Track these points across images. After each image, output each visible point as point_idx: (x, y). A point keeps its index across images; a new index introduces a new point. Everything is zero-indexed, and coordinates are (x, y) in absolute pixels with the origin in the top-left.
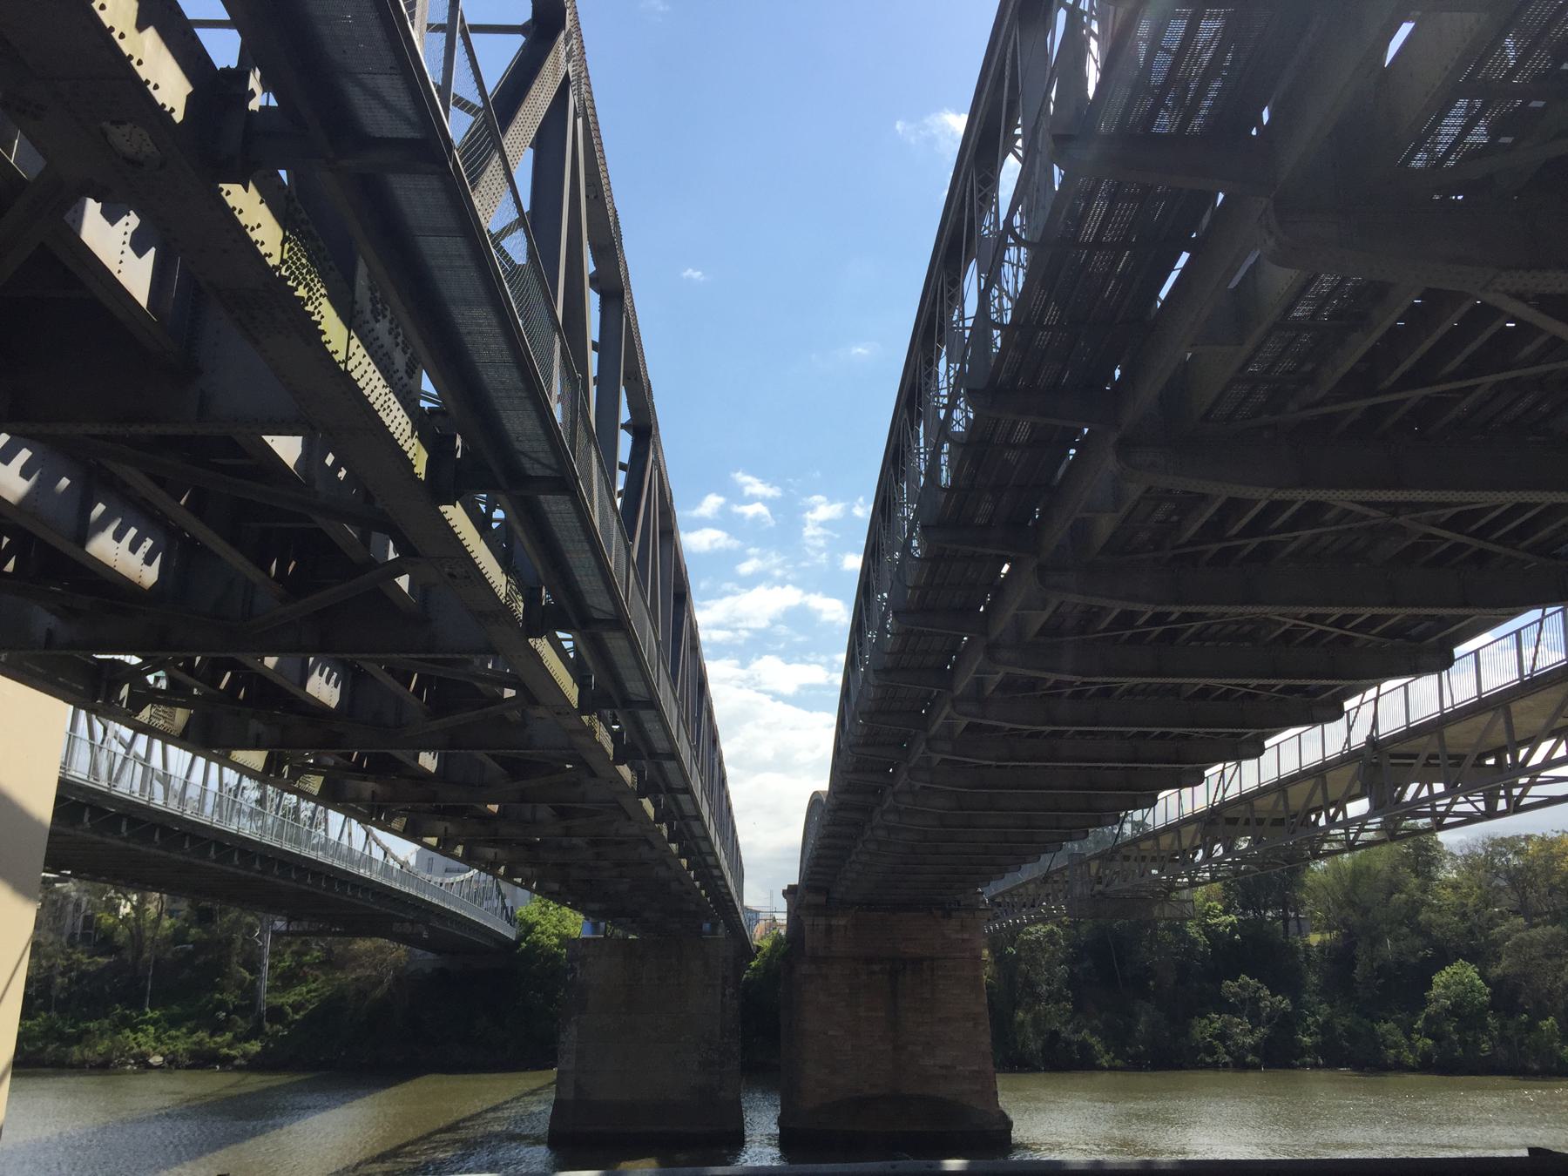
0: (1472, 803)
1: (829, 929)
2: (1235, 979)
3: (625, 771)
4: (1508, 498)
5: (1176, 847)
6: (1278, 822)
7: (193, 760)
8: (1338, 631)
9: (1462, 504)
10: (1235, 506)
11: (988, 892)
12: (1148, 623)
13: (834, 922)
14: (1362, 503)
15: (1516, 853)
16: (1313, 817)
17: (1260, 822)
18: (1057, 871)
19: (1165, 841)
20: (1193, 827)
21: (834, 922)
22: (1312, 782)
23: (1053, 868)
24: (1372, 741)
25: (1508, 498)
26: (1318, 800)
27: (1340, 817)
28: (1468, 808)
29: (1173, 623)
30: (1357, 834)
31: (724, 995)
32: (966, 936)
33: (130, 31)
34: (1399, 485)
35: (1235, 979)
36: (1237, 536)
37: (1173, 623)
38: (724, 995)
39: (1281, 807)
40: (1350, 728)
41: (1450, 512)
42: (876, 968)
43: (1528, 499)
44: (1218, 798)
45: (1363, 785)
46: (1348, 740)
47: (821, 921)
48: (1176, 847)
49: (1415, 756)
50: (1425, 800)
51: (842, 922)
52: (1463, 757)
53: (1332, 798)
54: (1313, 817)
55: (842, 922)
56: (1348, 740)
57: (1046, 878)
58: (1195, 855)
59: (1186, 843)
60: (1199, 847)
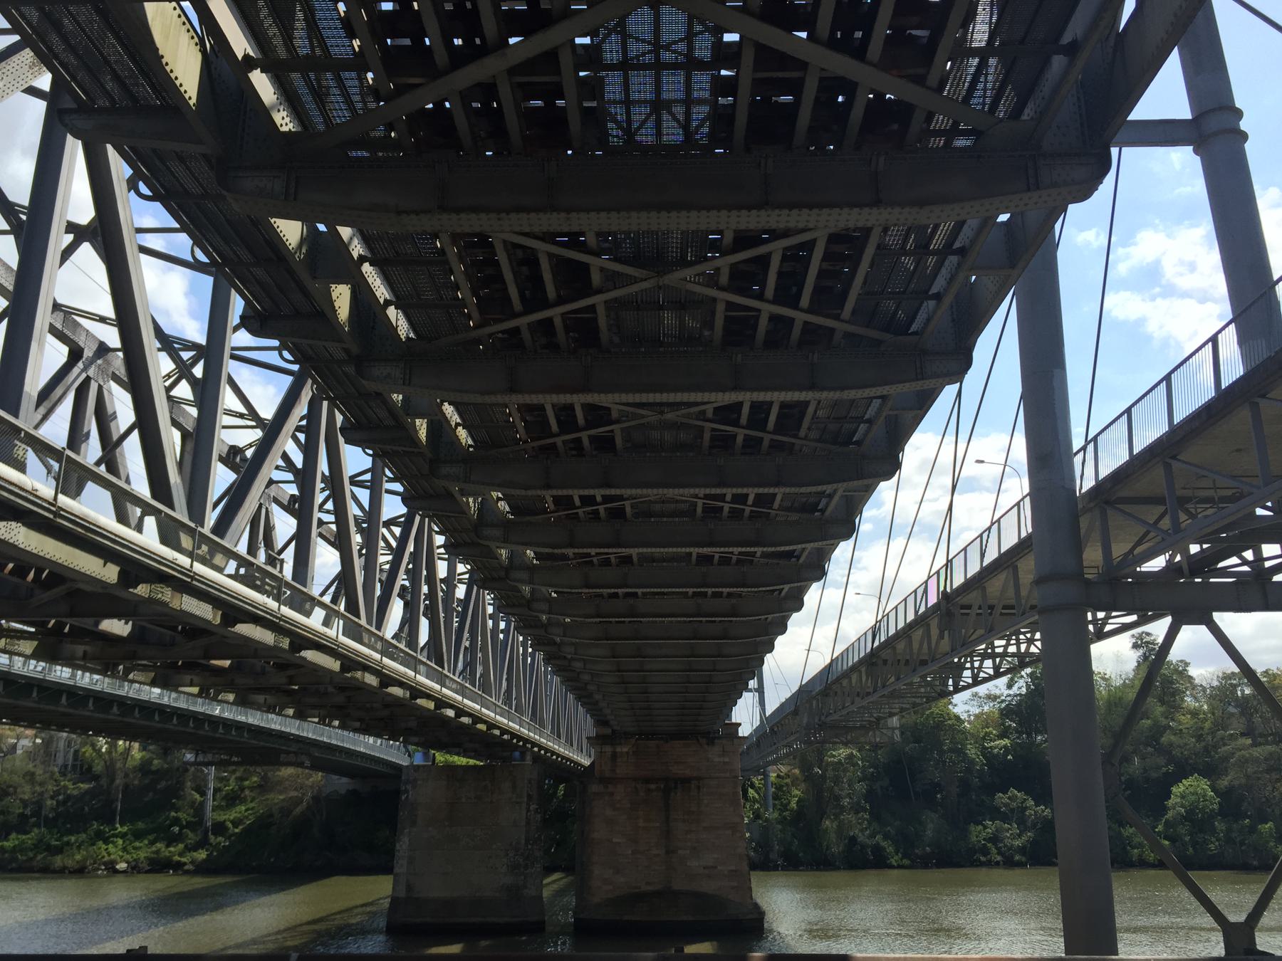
1: (614, 756)
13: (618, 749)
21: (618, 749)
31: (528, 810)
39: (1011, 592)
42: (653, 786)
47: (608, 749)
55: (625, 750)
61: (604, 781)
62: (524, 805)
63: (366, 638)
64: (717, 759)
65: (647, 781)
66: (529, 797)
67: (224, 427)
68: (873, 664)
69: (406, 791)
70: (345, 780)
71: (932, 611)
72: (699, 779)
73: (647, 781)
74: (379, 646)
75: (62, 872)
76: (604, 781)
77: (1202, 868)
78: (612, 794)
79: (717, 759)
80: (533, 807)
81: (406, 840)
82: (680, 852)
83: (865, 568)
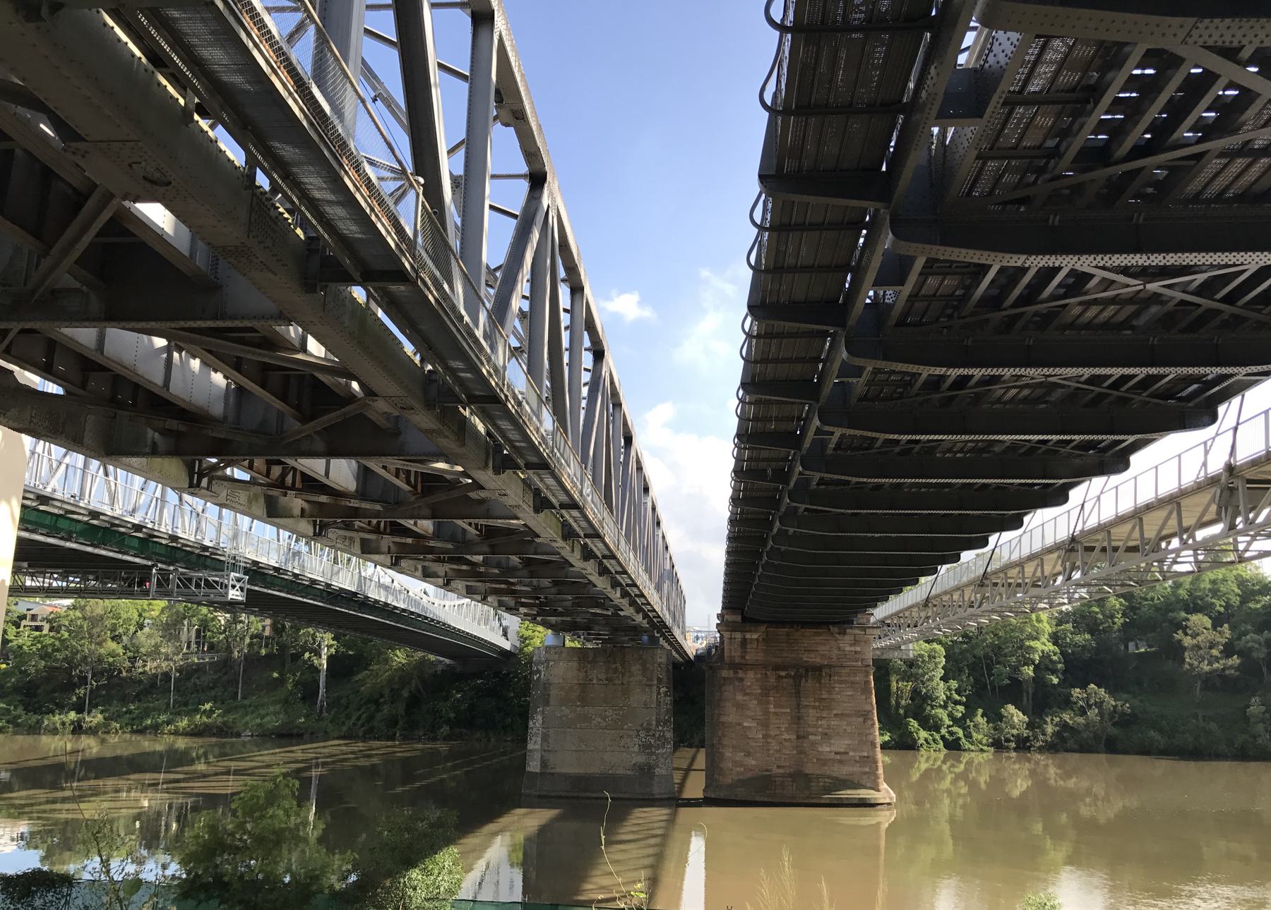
1: (744, 642)
2: (1084, 686)
3: (299, 231)
5: (1039, 574)
6: (1134, 549)
7: (86, 466)
8: (1115, 393)
11: (880, 612)
13: (748, 636)
15: (1017, 613)
18: (937, 596)
19: (1029, 569)
21: (748, 636)
22: (1170, 507)
23: (933, 592)
24: (1230, 469)
27: (1190, 541)
29: (971, 388)
30: (1170, 567)
31: (659, 693)
32: (858, 649)
33: (609, 589)
35: (1084, 686)
36: (1014, 306)
37: (971, 388)
38: (659, 693)
39: (1136, 534)
41: (1201, 278)
42: (783, 674)
44: (1079, 528)
45: (1219, 513)
46: (1205, 464)
47: (738, 635)
48: (1039, 574)
51: (755, 636)
53: (1185, 524)
55: (755, 636)
56: (1205, 464)
57: (927, 603)
59: (1048, 569)
60: (1059, 573)
61: (735, 667)
64: (848, 648)
65: (777, 668)
66: (659, 680)
67: (515, 216)
68: (1072, 550)
71: (1213, 481)
72: (830, 667)
73: (777, 668)
74: (269, 579)
75: (832, 778)
78: (742, 680)
79: (848, 648)
81: (540, 717)
82: (811, 737)
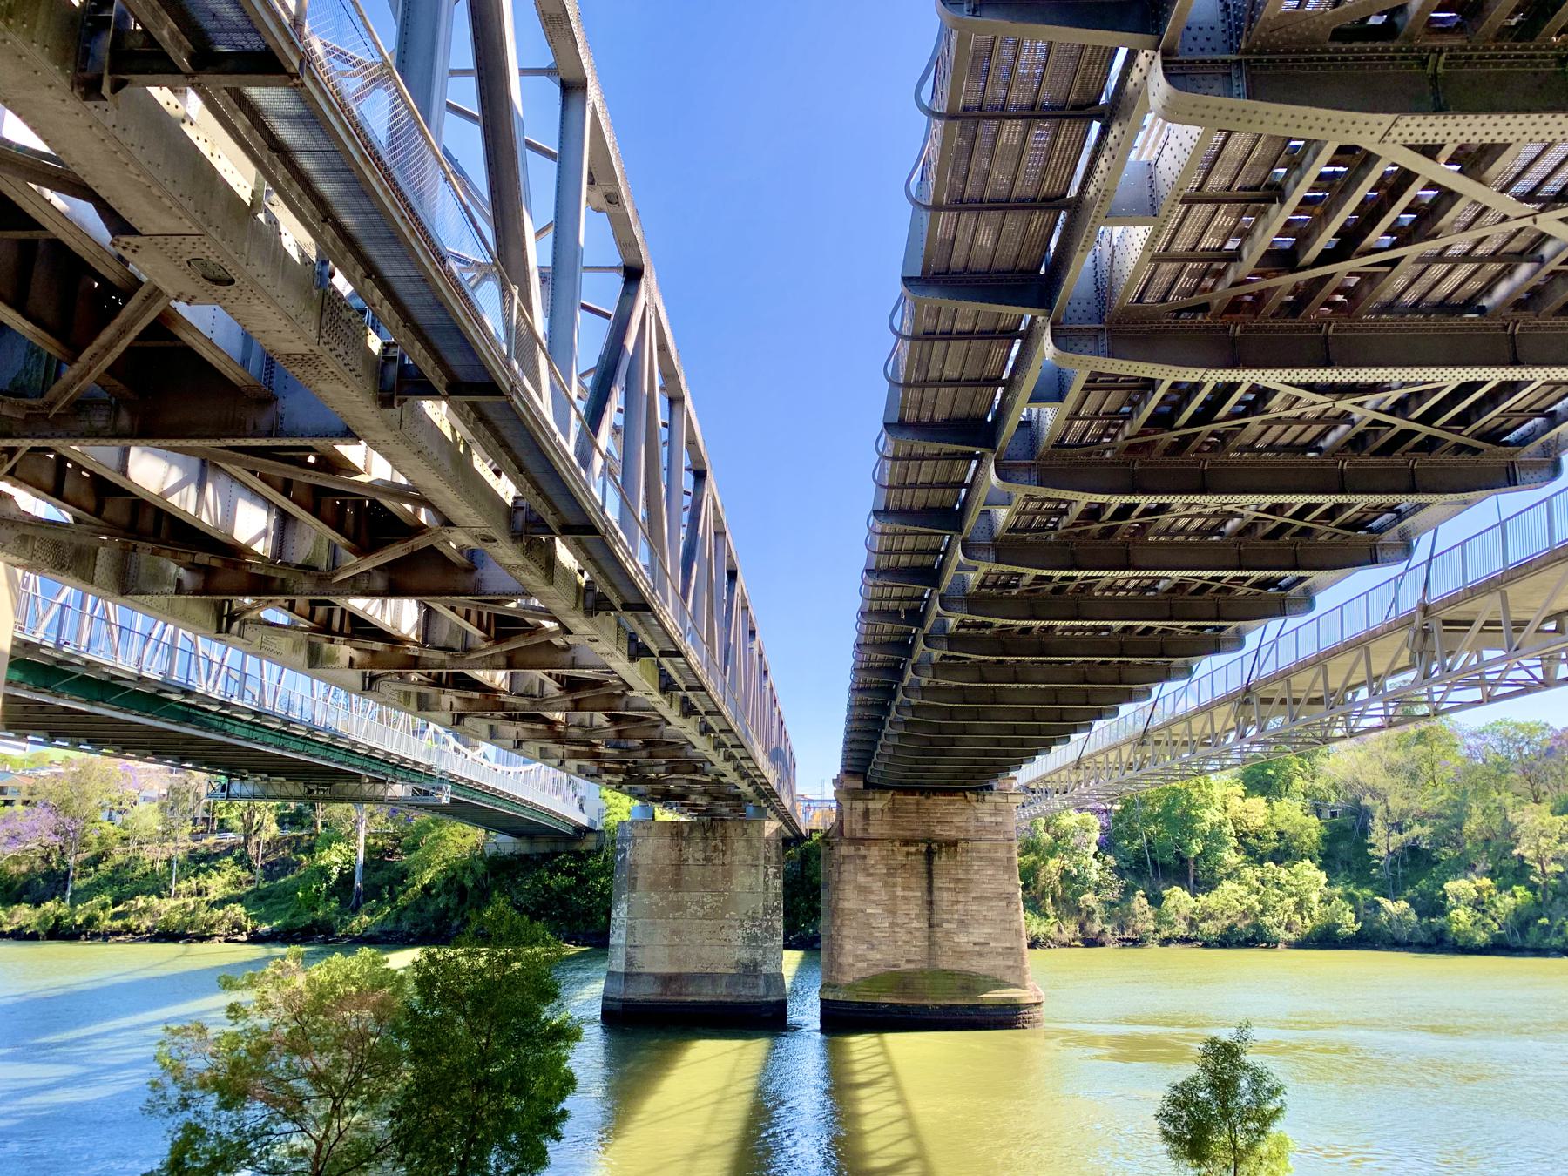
0: (1527, 669)
1: (866, 814)
4: (1451, 378)
5: (1208, 731)
6: (1318, 701)
9: (1414, 384)
10: (1185, 392)
12: (1114, 517)
13: (871, 805)
14: (1299, 386)
16: (1350, 695)
17: (1296, 701)
18: (1091, 756)
20: (1227, 708)
21: (871, 805)
25: (1451, 378)
26: (1360, 675)
28: (1522, 675)
31: (766, 875)
32: (999, 819)
34: (1328, 364)
38: (766, 875)
39: (1320, 685)
40: (1395, 600)
41: (1395, 396)
42: (913, 849)
43: (1518, 377)
47: (859, 804)
49: (1470, 623)
50: (1474, 667)
51: (879, 805)
52: (1526, 623)
53: (1375, 672)
54: (1350, 695)
55: (879, 805)
58: (1226, 738)
61: (856, 841)
62: (761, 869)
63: (1038, 716)
64: (988, 819)
66: (767, 859)
69: (624, 851)
70: (511, 839)
76: (856, 841)
77: (555, 238)
78: (864, 857)
80: (771, 871)
81: (624, 906)
83: (1243, 1028)
